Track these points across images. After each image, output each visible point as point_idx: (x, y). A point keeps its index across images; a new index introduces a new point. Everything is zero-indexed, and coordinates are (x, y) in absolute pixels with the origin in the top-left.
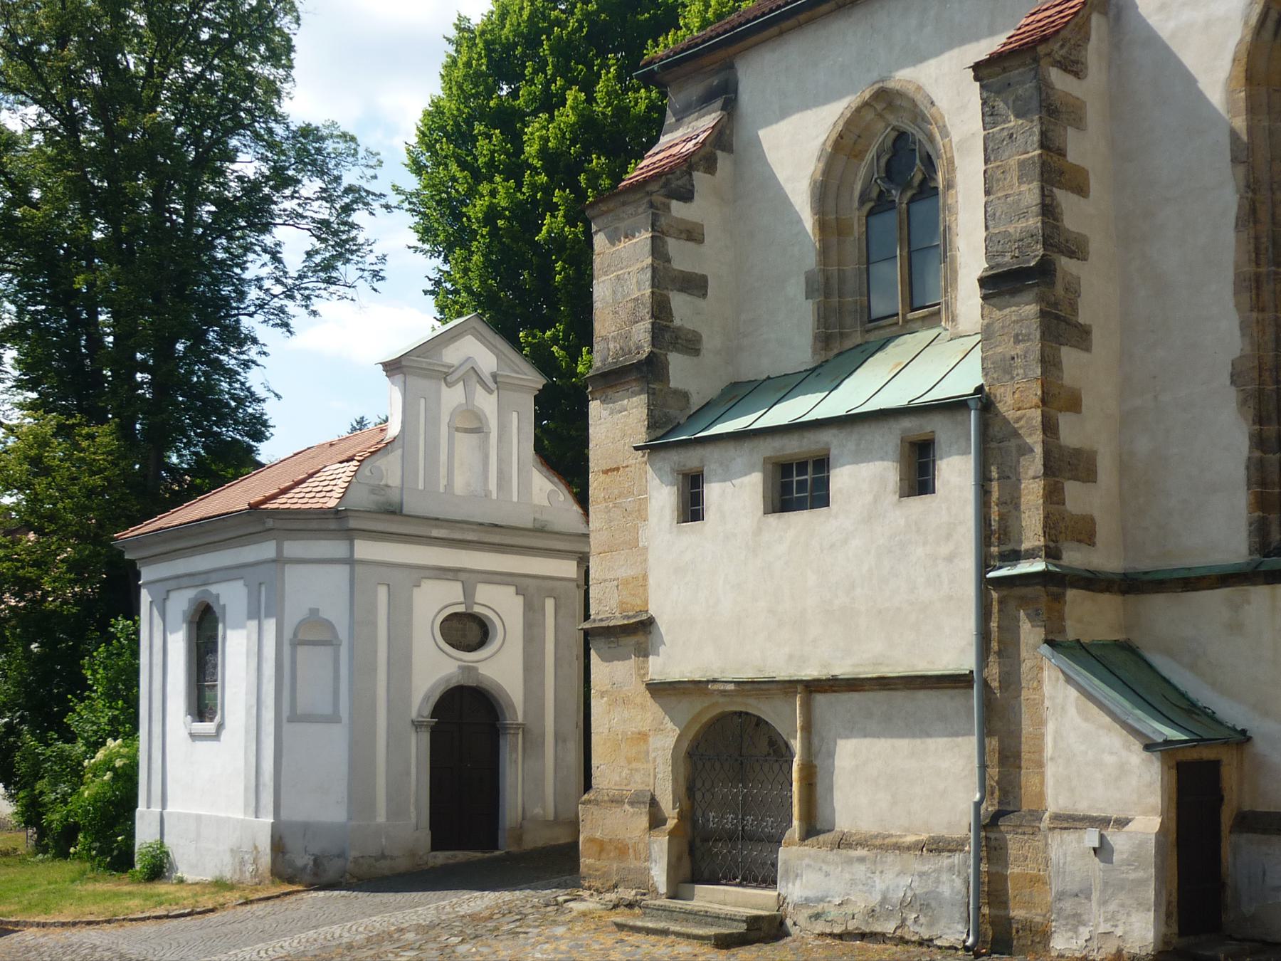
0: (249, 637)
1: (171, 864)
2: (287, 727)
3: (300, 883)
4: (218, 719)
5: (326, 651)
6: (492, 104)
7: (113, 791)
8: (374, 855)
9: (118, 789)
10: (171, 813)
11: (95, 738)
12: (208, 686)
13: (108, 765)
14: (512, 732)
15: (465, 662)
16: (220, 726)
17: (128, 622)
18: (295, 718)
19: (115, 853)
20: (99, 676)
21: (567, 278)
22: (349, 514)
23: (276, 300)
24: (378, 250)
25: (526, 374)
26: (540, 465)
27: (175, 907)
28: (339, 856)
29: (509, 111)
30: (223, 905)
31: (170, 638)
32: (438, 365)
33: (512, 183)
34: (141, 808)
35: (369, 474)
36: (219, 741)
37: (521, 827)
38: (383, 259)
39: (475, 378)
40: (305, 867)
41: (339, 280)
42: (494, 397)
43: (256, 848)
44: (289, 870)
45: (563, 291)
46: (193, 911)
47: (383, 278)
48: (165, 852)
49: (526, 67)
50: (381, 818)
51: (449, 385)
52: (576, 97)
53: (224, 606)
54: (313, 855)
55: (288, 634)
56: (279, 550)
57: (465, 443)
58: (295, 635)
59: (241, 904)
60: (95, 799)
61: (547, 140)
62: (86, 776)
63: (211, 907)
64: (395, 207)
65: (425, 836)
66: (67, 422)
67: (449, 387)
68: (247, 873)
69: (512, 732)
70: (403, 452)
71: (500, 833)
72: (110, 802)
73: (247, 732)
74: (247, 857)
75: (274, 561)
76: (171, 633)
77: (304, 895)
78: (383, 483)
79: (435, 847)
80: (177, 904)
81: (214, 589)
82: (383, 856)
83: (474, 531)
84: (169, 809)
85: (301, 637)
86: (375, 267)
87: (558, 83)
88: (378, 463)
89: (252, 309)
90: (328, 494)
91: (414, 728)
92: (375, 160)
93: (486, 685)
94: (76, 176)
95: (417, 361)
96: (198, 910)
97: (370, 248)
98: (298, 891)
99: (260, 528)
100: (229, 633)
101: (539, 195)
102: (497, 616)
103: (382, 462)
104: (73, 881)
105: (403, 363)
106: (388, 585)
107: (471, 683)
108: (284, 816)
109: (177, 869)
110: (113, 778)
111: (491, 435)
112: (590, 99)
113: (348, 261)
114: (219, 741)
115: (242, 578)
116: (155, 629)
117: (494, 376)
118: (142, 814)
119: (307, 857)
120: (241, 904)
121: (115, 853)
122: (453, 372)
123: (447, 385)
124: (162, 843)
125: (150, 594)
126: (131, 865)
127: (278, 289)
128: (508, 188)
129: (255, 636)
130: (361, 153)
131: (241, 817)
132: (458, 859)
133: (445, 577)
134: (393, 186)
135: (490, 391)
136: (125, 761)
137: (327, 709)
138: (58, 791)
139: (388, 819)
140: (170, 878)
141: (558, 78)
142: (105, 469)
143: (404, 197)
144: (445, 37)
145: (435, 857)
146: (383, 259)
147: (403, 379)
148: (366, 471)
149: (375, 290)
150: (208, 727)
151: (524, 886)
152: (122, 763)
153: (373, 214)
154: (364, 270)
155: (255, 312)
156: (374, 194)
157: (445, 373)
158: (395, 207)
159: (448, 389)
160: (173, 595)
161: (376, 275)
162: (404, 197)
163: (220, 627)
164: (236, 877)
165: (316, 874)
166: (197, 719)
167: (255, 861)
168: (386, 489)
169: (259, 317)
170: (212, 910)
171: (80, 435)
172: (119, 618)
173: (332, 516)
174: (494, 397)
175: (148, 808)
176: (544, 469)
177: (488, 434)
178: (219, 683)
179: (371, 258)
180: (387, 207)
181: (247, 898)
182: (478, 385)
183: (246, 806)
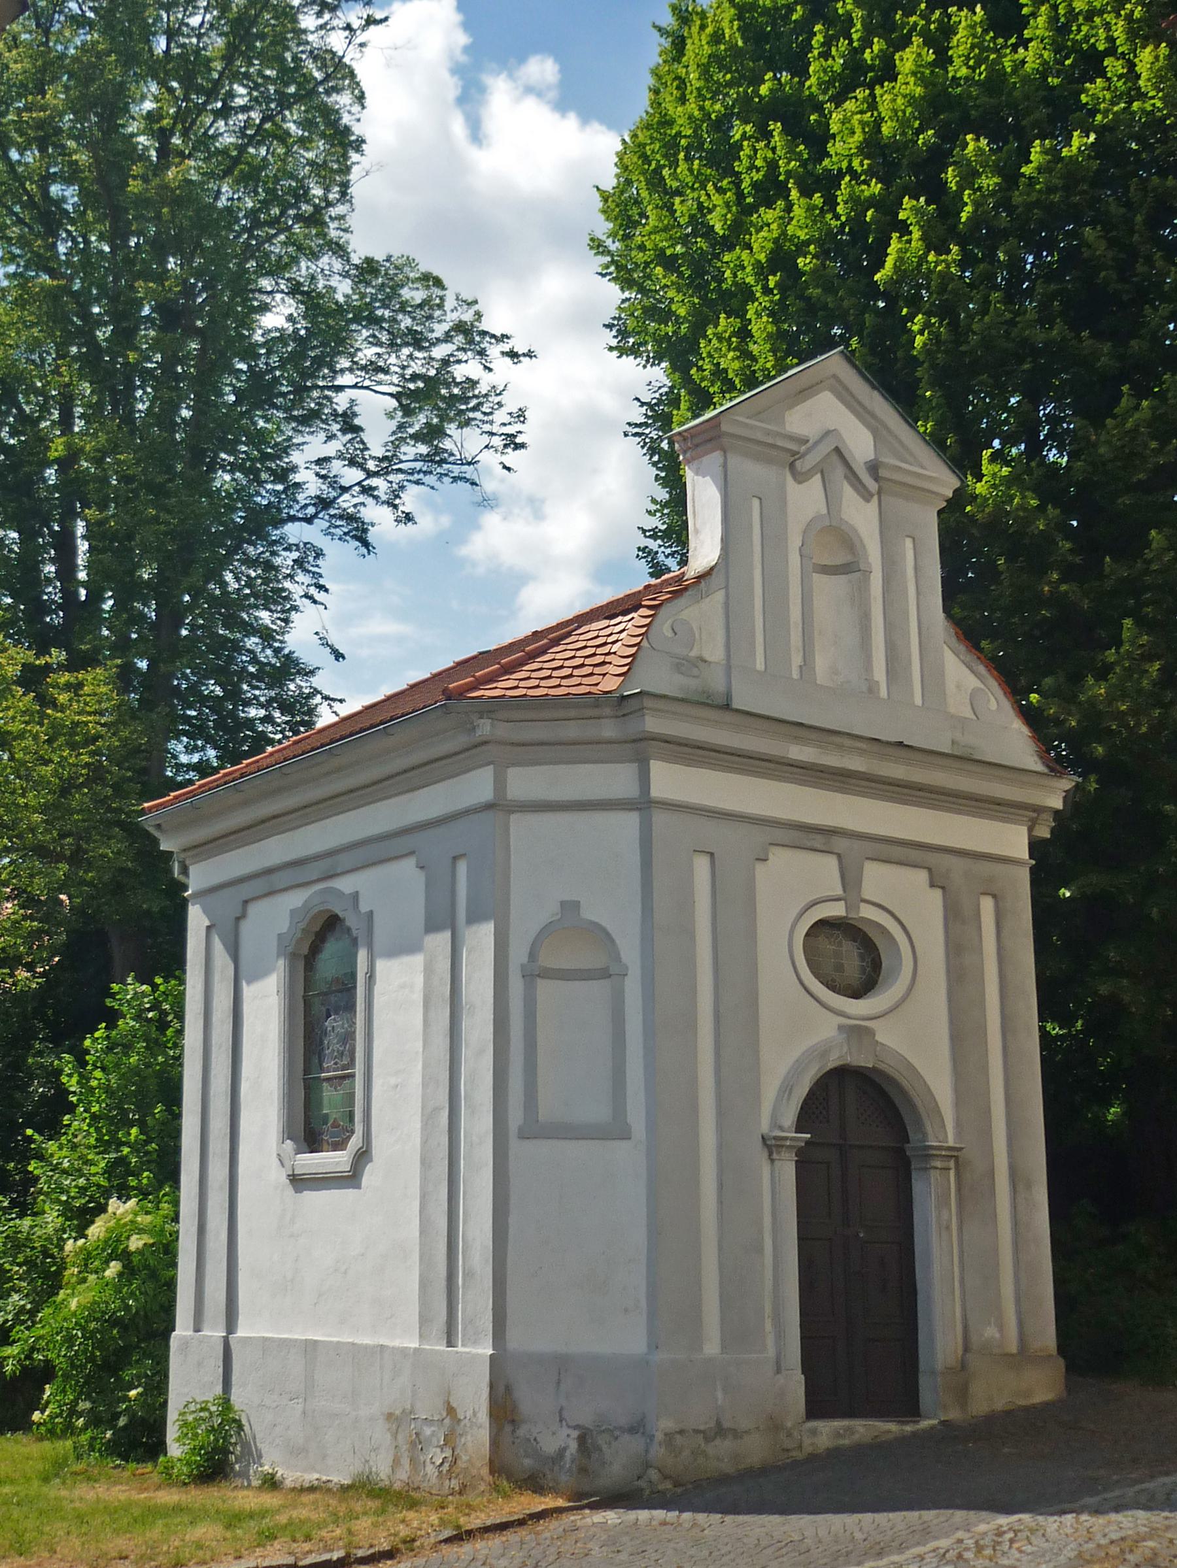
0: (428, 971)
1: (246, 1445)
2: (516, 1147)
3: (555, 1491)
4: (355, 1142)
5: (598, 989)
6: (764, 90)
7: (123, 1300)
8: (702, 1428)
9: (132, 1294)
10: (246, 1340)
11: (83, 1201)
12: (328, 1079)
13: (114, 1249)
14: (938, 1164)
15: (849, 1017)
16: (363, 1156)
17: (144, 987)
18: (534, 1130)
19: (122, 1422)
20: (94, 1083)
21: (936, 339)
22: (648, 702)
23: (346, 496)
24: (511, 403)
25: (922, 467)
26: (954, 639)
27: (307, 1546)
28: (632, 1430)
29: (794, 99)
30: (410, 1541)
31: (249, 991)
32: (779, 434)
33: (817, 199)
34: (182, 1330)
35: (669, 634)
36: (358, 1187)
37: (963, 1366)
38: (521, 416)
39: (840, 471)
40: (561, 1452)
41: (452, 454)
42: (873, 507)
43: (451, 1410)
44: (527, 1462)
45: (925, 365)
46: (348, 1555)
47: (522, 446)
48: (235, 1421)
49: (815, 34)
50: (712, 1347)
51: (800, 477)
52: (919, 55)
53: (370, 914)
54: (576, 1427)
55: (518, 954)
56: (500, 784)
57: (829, 589)
58: (533, 955)
59: (447, 1541)
60: (93, 1311)
61: (878, 122)
62: (67, 1273)
63: (386, 1546)
64: (524, 355)
65: (795, 1384)
66: (38, 662)
67: (800, 483)
68: (430, 1469)
69: (938, 1164)
70: (727, 596)
71: (924, 1382)
72: (115, 1322)
73: (425, 1163)
74: (428, 1431)
75: (489, 806)
76: (248, 983)
77: (573, 1517)
78: (693, 654)
79: (816, 1408)
80: (308, 1538)
81: (345, 885)
82: (720, 1431)
83: (862, 752)
84: (243, 1331)
85: (548, 960)
86: (510, 430)
87: (876, 48)
88: (684, 615)
89: (311, 510)
90: (597, 670)
91: (766, 1154)
92: (471, 312)
93: (889, 1066)
94: (58, 287)
95: (746, 425)
96: (360, 1553)
97: (497, 399)
98: (559, 1511)
99: (462, 740)
100: (381, 965)
101: (869, 213)
102: (899, 927)
103: (688, 611)
104: (46, 1480)
105: (725, 427)
106: (712, 854)
107: (862, 1059)
108: (516, 1341)
109: (260, 1457)
110: (120, 1275)
111: (872, 575)
112: (942, 59)
113: (467, 423)
114: (358, 1187)
115: (412, 853)
116: (217, 977)
117: (874, 468)
118: (185, 1343)
119: (566, 1431)
120: (447, 1541)
121: (122, 1422)
122: (808, 451)
123: (795, 479)
124: (225, 1402)
125: (206, 911)
126: (156, 1448)
127: (352, 476)
128: (810, 209)
129: (444, 965)
130: (450, 303)
131: (414, 1344)
132: (856, 1437)
133: (809, 844)
134: (592, 240)
135: (866, 496)
136: (148, 1239)
137: (596, 1111)
138: (10, 1308)
139: (724, 1348)
140: (244, 1474)
141: (876, 40)
142: (95, 739)
143: (609, 259)
144: (655, 26)
145: (814, 1432)
146: (521, 416)
147: (721, 460)
148: (664, 626)
149: (509, 469)
150: (334, 1160)
151: (1066, 1506)
152: (141, 1244)
153: (490, 370)
154: (492, 434)
155: (315, 516)
156: (493, 336)
157: (794, 453)
158: (524, 355)
159: (796, 485)
160: (254, 909)
161: (513, 443)
162: (609, 259)
163: (362, 955)
164: (403, 1475)
165: (583, 1470)
166: (305, 1146)
167: (450, 1440)
168: (701, 664)
169: (321, 524)
170: (390, 1555)
171: (56, 686)
172: (129, 980)
173: (607, 711)
174: (873, 507)
175: (197, 1330)
176: (962, 648)
177: (867, 573)
178: (359, 1070)
179: (500, 416)
180: (513, 355)
181: (458, 1527)
182: (845, 483)
183: (424, 1320)
